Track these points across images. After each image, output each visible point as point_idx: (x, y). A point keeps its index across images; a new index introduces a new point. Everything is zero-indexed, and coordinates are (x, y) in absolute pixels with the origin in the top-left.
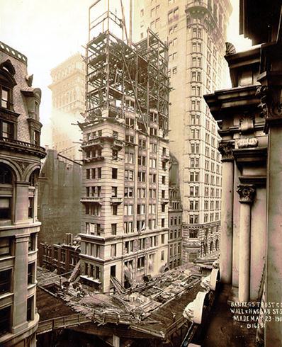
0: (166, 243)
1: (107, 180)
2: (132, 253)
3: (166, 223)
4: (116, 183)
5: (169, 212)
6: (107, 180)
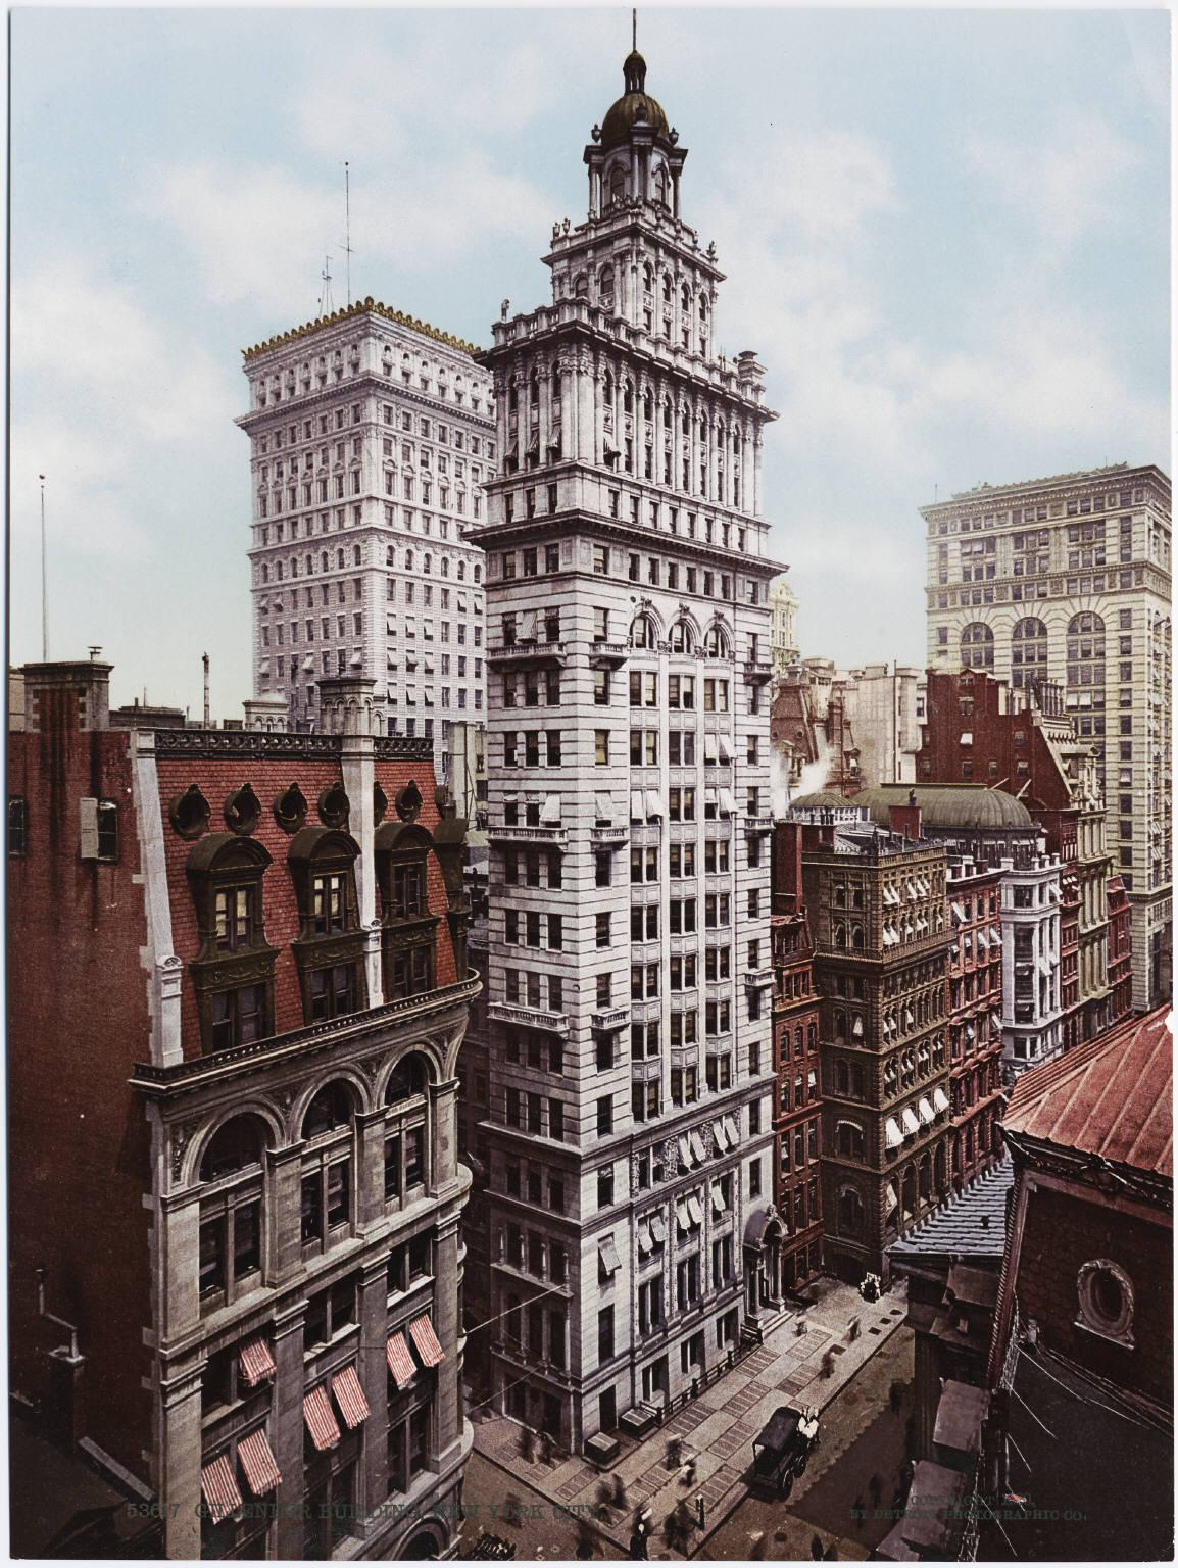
0: (766, 1127)
1: (581, 772)
2: (660, 1186)
3: (766, 1057)
4: (603, 717)
5: (774, 1016)
6: (581, 711)
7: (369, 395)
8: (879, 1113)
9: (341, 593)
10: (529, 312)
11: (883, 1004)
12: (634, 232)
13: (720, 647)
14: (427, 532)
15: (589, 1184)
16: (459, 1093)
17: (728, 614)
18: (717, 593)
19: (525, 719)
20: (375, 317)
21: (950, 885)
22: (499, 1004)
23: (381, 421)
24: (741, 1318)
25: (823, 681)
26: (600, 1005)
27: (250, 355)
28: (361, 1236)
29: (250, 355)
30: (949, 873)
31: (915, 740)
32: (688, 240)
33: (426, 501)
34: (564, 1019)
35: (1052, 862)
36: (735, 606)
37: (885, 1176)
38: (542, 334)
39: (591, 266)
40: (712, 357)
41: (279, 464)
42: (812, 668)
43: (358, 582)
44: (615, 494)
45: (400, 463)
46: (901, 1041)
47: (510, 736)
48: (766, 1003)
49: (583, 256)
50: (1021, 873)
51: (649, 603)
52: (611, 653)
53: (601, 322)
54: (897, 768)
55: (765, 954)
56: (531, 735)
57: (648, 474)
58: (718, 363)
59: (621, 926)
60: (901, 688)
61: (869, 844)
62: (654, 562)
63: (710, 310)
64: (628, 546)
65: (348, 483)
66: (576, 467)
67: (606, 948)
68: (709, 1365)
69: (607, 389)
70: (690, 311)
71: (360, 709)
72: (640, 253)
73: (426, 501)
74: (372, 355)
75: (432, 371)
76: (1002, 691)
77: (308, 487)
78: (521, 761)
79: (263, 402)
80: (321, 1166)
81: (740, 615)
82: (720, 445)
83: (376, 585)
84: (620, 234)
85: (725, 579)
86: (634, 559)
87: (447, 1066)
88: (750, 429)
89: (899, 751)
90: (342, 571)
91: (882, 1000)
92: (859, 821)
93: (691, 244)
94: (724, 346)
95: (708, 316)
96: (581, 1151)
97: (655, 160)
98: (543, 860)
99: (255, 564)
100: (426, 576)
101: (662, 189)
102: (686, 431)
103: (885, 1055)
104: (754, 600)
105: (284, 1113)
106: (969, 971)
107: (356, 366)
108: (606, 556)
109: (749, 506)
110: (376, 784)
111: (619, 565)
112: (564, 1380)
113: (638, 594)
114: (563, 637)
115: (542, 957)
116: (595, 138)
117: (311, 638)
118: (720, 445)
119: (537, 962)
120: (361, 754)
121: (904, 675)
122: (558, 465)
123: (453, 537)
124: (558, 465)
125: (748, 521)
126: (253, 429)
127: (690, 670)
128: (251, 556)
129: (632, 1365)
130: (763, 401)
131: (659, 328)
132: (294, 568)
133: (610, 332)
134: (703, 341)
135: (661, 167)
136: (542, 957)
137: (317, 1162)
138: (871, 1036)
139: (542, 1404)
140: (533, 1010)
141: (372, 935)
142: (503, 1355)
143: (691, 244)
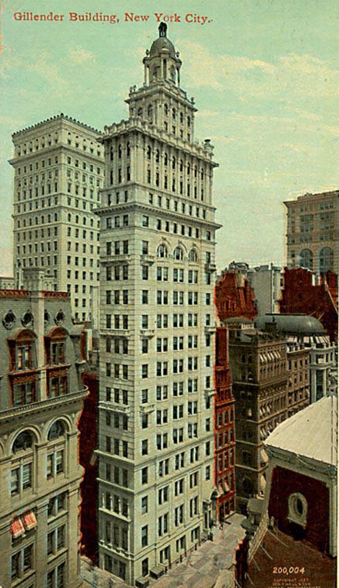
5: (216, 408)
7: (61, 152)
8: (258, 447)
9: (43, 234)
10: (118, 122)
11: (260, 401)
12: (161, 92)
13: (194, 255)
14: (77, 206)
15: (138, 475)
16: (79, 436)
17: (198, 244)
18: (194, 236)
19: (113, 286)
20: (64, 121)
21: (288, 354)
22: (103, 402)
23: (66, 163)
24: (202, 531)
25: (244, 272)
26: (143, 402)
27: (14, 136)
28: (36, 493)
29: (14, 136)
30: (288, 349)
31: (279, 296)
32: (182, 95)
33: (84, 195)
34: (128, 408)
35: (332, 345)
36: (201, 241)
37: (260, 472)
38: (123, 131)
39: (144, 104)
40: (193, 140)
41: (37, 176)
42: (239, 267)
43: (56, 228)
44: (151, 195)
45: (81, 181)
46: (267, 418)
47: (108, 292)
48: (212, 401)
49: (138, 101)
50: (319, 349)
51: (165, 239)
52: (149, 260)
53: (147, 126)
54: (271, 308)
55: (212, 382)
56: (116, 292)
57: (166, 187)
58: (195, 144)
59: (152, 370)
60: (274, 275)
61: (255, 339)
62: (167, 223)
63: (193, 123)
64: (157, 216)
65: (53, 188)
66: (135, 184)
67: (146, 379)
68: (188, 548)
69: (149, 153)
70: (184, 123)
71: (38, 280)
72: (163, 100)
73: (84, 195)
74: (63, 136)
75: (88, 143)
76: (313, 277)
77: (31, 190)
78: (113, 303)
79: (19, 154)
80: (20, 465)
81: (203, 244)
82: (196, 176)
83: (63, 230)
84: (155, 92)
85: (197, 230)
86: (159, 221)
87: (74, 425)
88: (208, 170)
89: (273, 300)
90: (37, 226)
91: (259, 401)
92: (253, 328)
93: (184, 96)
94: (199, 137)
95: (191, 125)
96: (135, 462)
97: (169, 63)
98: (113, 341)
99: (15, 220)
100: (85, 226)
101: (172, 75)
102: (181, 170)
103: (260, 424)
104: (209, 238)
105: (4, 443)
106: (302, 387)
107: (56, 141)
108: (148, 219)
109: (208, 201)
110: (45, 311)
111: (153, 224)
112: (127, 555)
113: (160, 236)
114: (129, 253)
115: (120, 382)
116: (147, 54)
117: (49, 250)
118: (196, 176)
119: (119, 384)
120: (38, 298)
121: (276, 270)
122: (129, 183)
123: (88, 209)
124: (129, 183)
125: (207, 207)
126: (15, 165)
127: (182, 267)
128: (13, 217)
129: (155, 549)
130: (214, 160)
131: (170, 130)
132: (49, 219)
133: (151, 131)
134: (189, 135)
135: (172, 66)
136: (120, 382)
137: (18, 463)
138: (254, 417)
139: (118, 566)
140: (116, 404)
141: (42, 371)
142: (104, 546)
143: (184, 96)
